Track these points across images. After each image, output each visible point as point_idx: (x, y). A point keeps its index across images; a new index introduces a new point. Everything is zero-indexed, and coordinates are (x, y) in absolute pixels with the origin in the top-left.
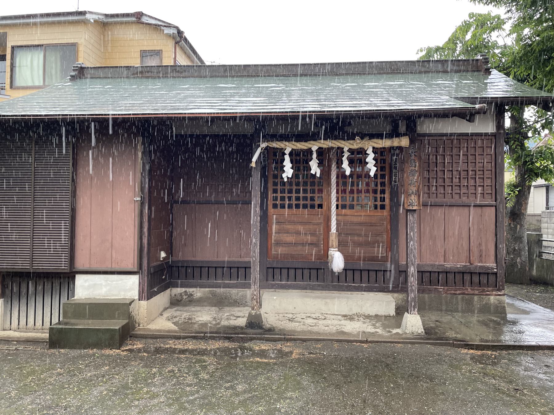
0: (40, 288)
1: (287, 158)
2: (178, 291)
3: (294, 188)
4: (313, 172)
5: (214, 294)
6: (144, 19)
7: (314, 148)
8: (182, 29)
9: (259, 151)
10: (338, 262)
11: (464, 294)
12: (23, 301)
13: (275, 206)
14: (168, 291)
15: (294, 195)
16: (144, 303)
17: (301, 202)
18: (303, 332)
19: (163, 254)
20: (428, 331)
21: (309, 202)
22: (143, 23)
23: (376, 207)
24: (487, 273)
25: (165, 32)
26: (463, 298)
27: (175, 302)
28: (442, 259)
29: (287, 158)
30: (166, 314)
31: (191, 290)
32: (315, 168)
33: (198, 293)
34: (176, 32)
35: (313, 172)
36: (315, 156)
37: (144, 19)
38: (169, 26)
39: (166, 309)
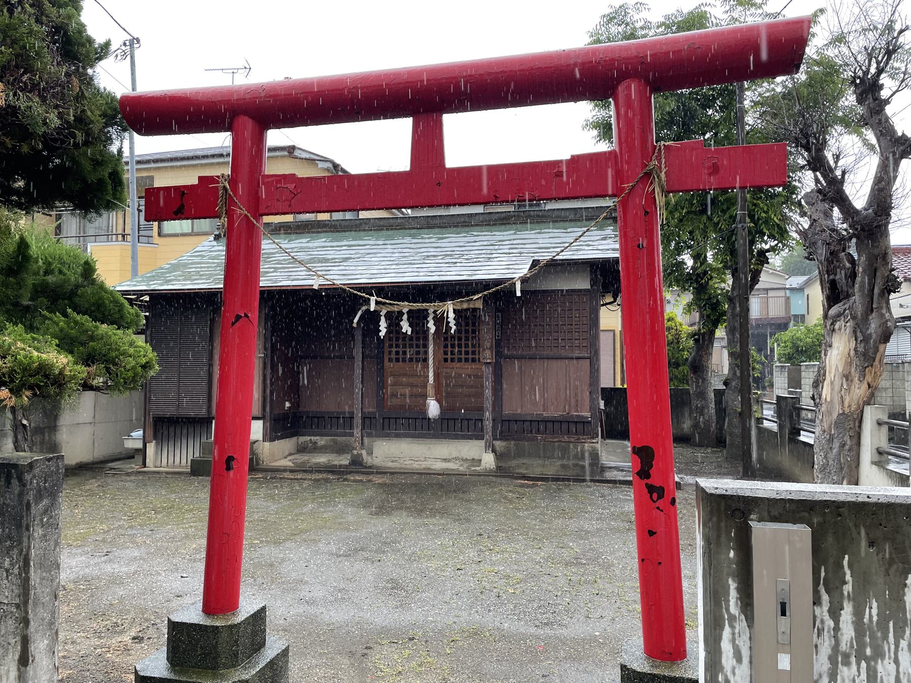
0: (185, 431)
1: (383, 319)
2: (302, 439)
3: (415, 342)
4: (404, 331)
5: (335, 442)
6: (297, 153)
7: (405, 310)
8: (337, 161)
9: (359, 313)
10: (433, 409)
11: (560, 441)
12: (171, 449)
13: (390, 360)
14: (295, 439)
15: (394, 350)
16: (267, 444)
17: (470, 356)
18: (400, 468)
19: (287, 404)
20: (499, 468)
21: (449, 356)
22: (296, 158)
23: (446, 360)
24: (584, 422)
25: (320, 166)
26: (559, 446)
27: (302, 449)
28: (542, 408)
29: (383, 319)
30: (289, 458)
31: (316, 438)
32: (406, 327)
33: (322, 441)
34: (330, 165)
35: (404, 331)
36: (405, 317)
37: (297, 153)
38: (326, 160)
39: (290, 454)
